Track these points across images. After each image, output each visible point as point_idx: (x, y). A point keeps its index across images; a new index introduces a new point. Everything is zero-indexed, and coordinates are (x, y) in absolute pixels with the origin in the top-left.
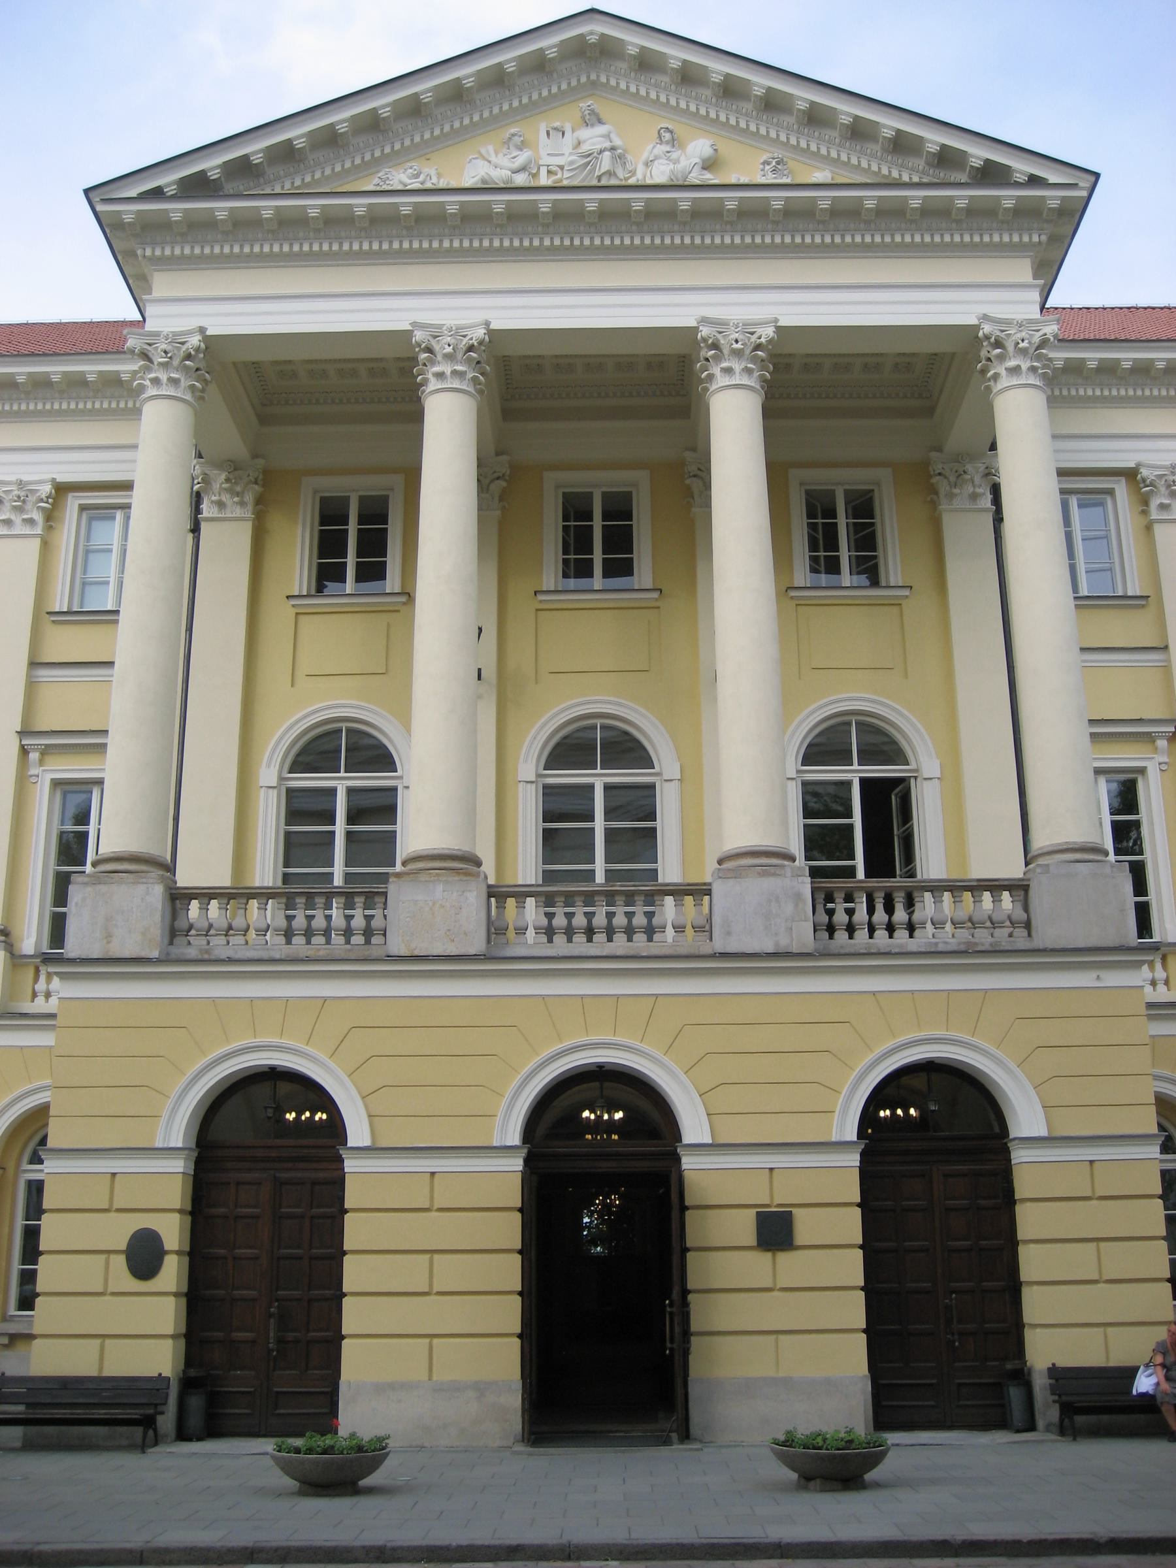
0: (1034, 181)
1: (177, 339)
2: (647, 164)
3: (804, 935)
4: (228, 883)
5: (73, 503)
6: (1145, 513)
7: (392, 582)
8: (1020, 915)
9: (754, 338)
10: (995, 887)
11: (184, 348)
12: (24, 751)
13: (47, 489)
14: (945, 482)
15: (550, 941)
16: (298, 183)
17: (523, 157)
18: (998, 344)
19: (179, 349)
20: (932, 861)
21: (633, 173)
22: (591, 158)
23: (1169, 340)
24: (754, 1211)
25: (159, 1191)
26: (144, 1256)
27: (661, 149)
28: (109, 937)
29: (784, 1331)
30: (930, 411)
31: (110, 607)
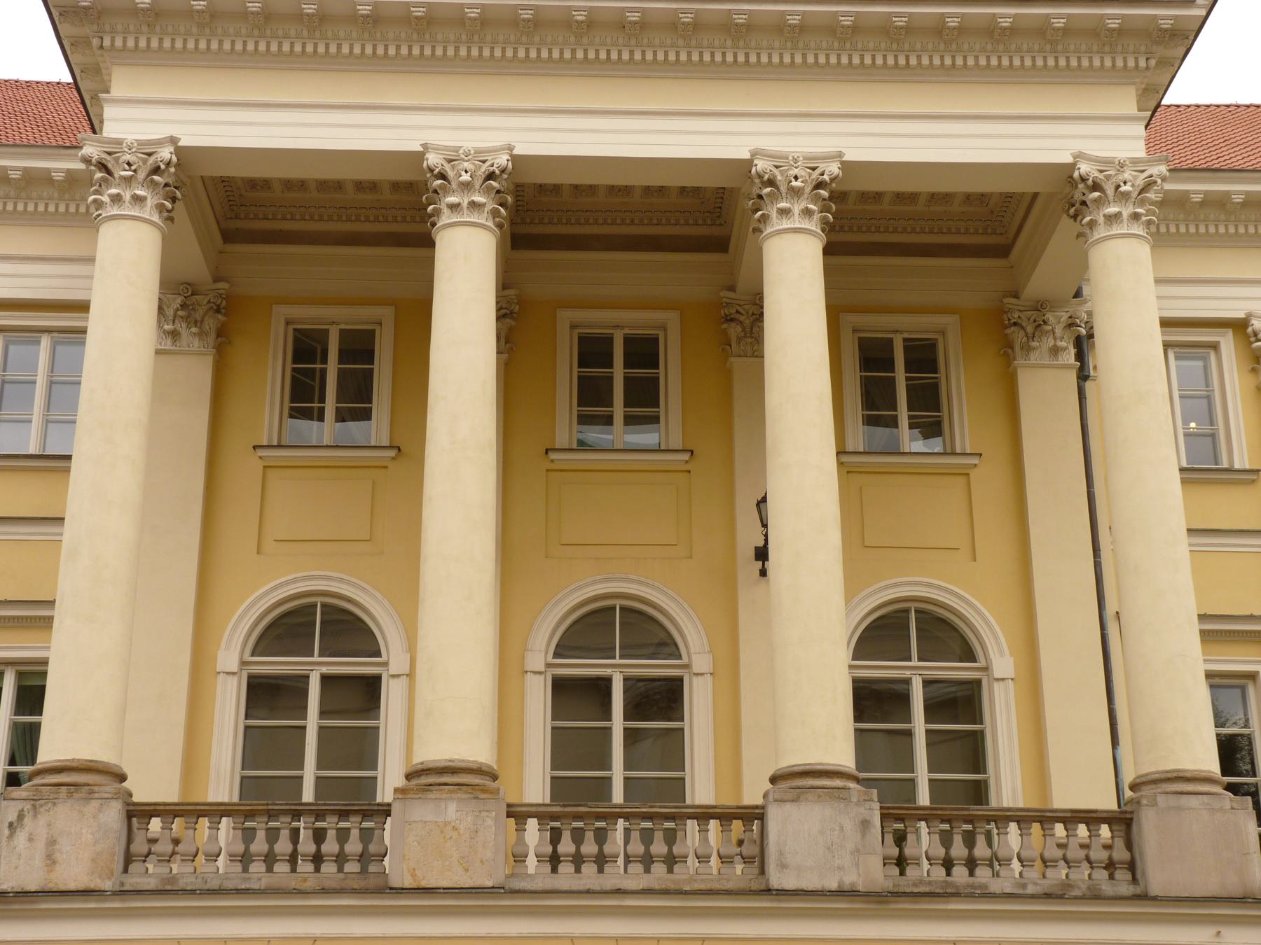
1: (147, 149)
4: (175, 799)
8: (1120, 854)
9: (816, 174)
10: (1092, 818)
11: (151, 160)
14: (1022, 333)
15: (554, 870)
18: (1096, 187)
19: (145, 162)
23: (1254, 171)
30: (1003, 251)
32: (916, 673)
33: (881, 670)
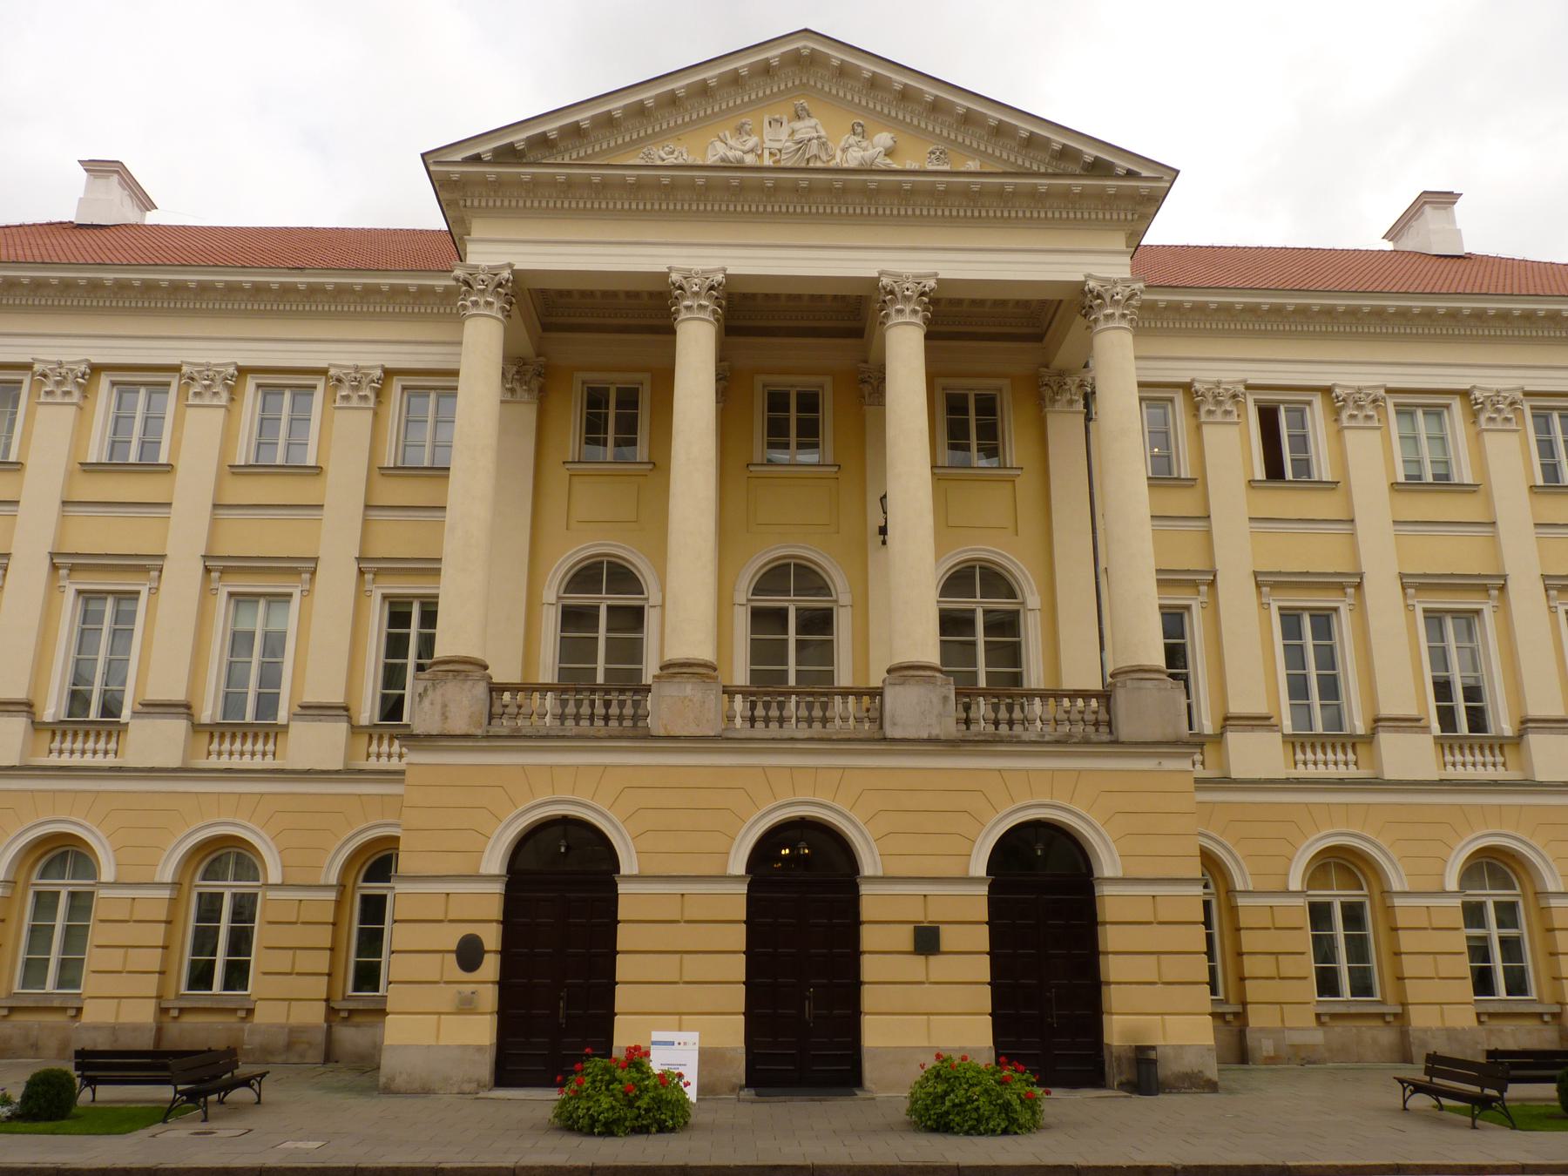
0: (1130, 174)
1: (494, 271)
2: (844, 150)
3: (950, 728)
4: (518, 680)
5: (397, 384)
6: (1196, 415)
7: (642, 451)
8: (1103, 716)
10: (1086, 695)
12: (361, 572)
13: (378, 373)
16: (582, 154)
17: (752, 141)
18: (1099, 296)
20: (1035, 675)
21: (833, 157)
22: (802, 144)
24: (911, 927)
25: (482, 907)
26: (469, 954)
27: (853, 139)
28: (445, 717)
29: (926, 1011)
30: (1039, 338)
31: (311, 462)
32: (979, 606)
33: (958, 603)
